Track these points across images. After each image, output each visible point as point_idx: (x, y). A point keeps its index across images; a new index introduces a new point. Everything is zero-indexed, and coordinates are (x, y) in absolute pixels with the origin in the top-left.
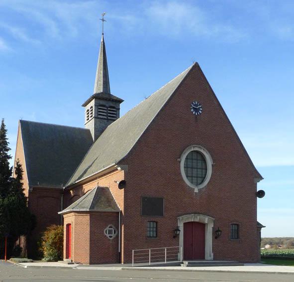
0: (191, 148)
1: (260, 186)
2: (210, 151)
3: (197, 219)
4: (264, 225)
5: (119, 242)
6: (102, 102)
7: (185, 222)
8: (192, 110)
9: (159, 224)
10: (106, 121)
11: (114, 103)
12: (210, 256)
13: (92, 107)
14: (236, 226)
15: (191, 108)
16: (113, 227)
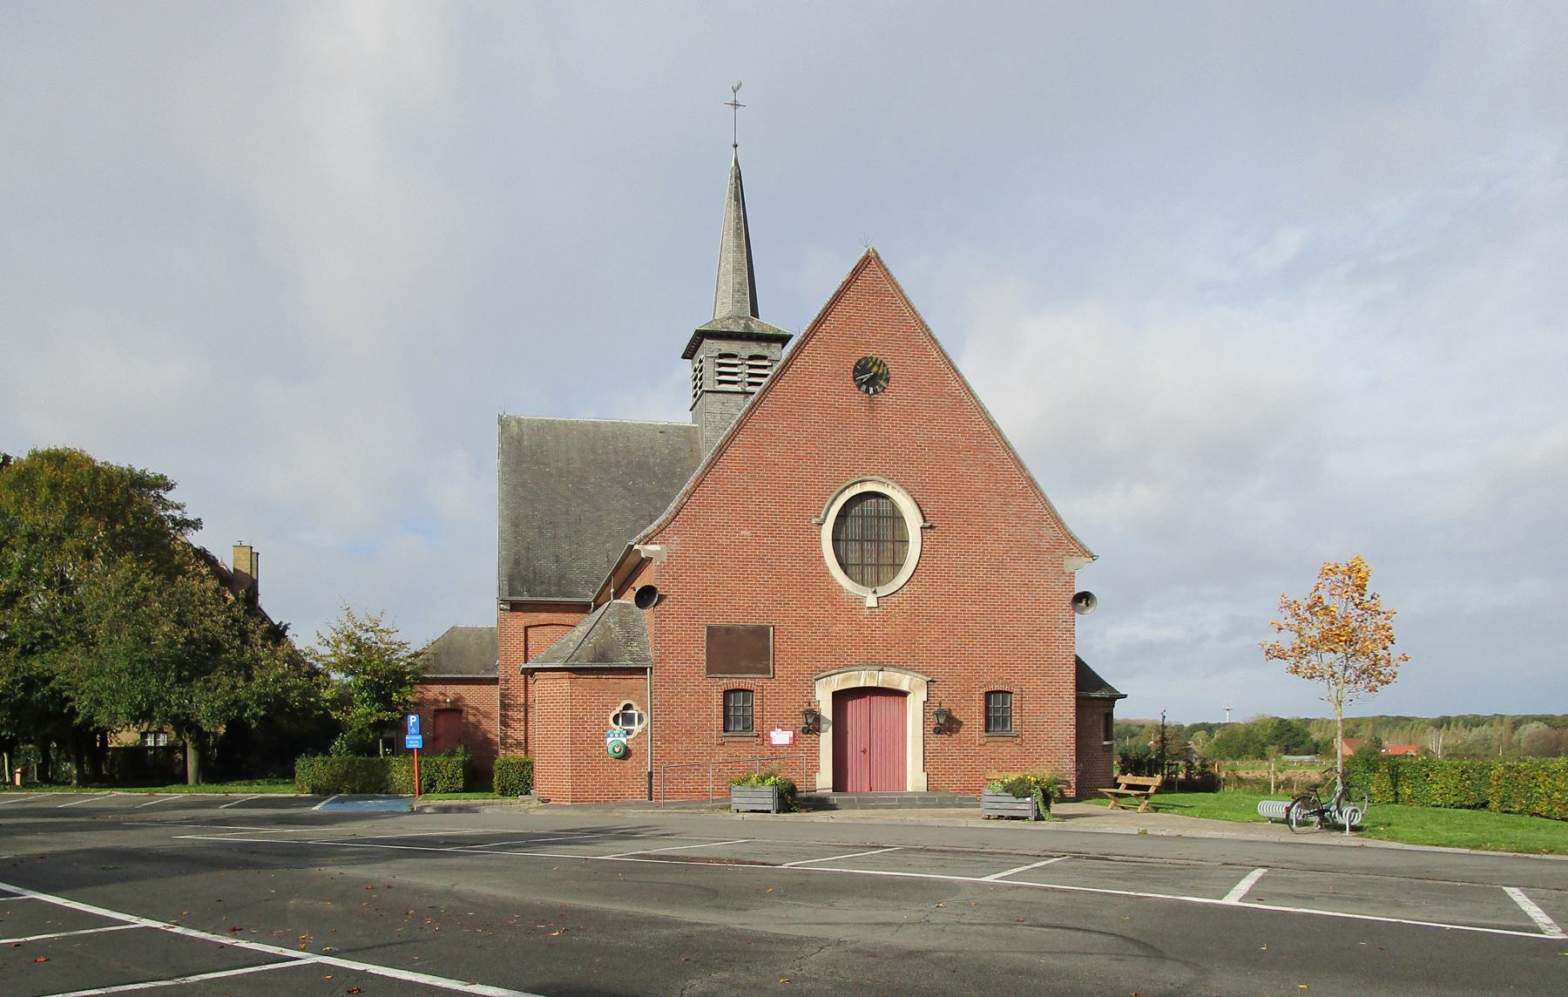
13: (701, 362)
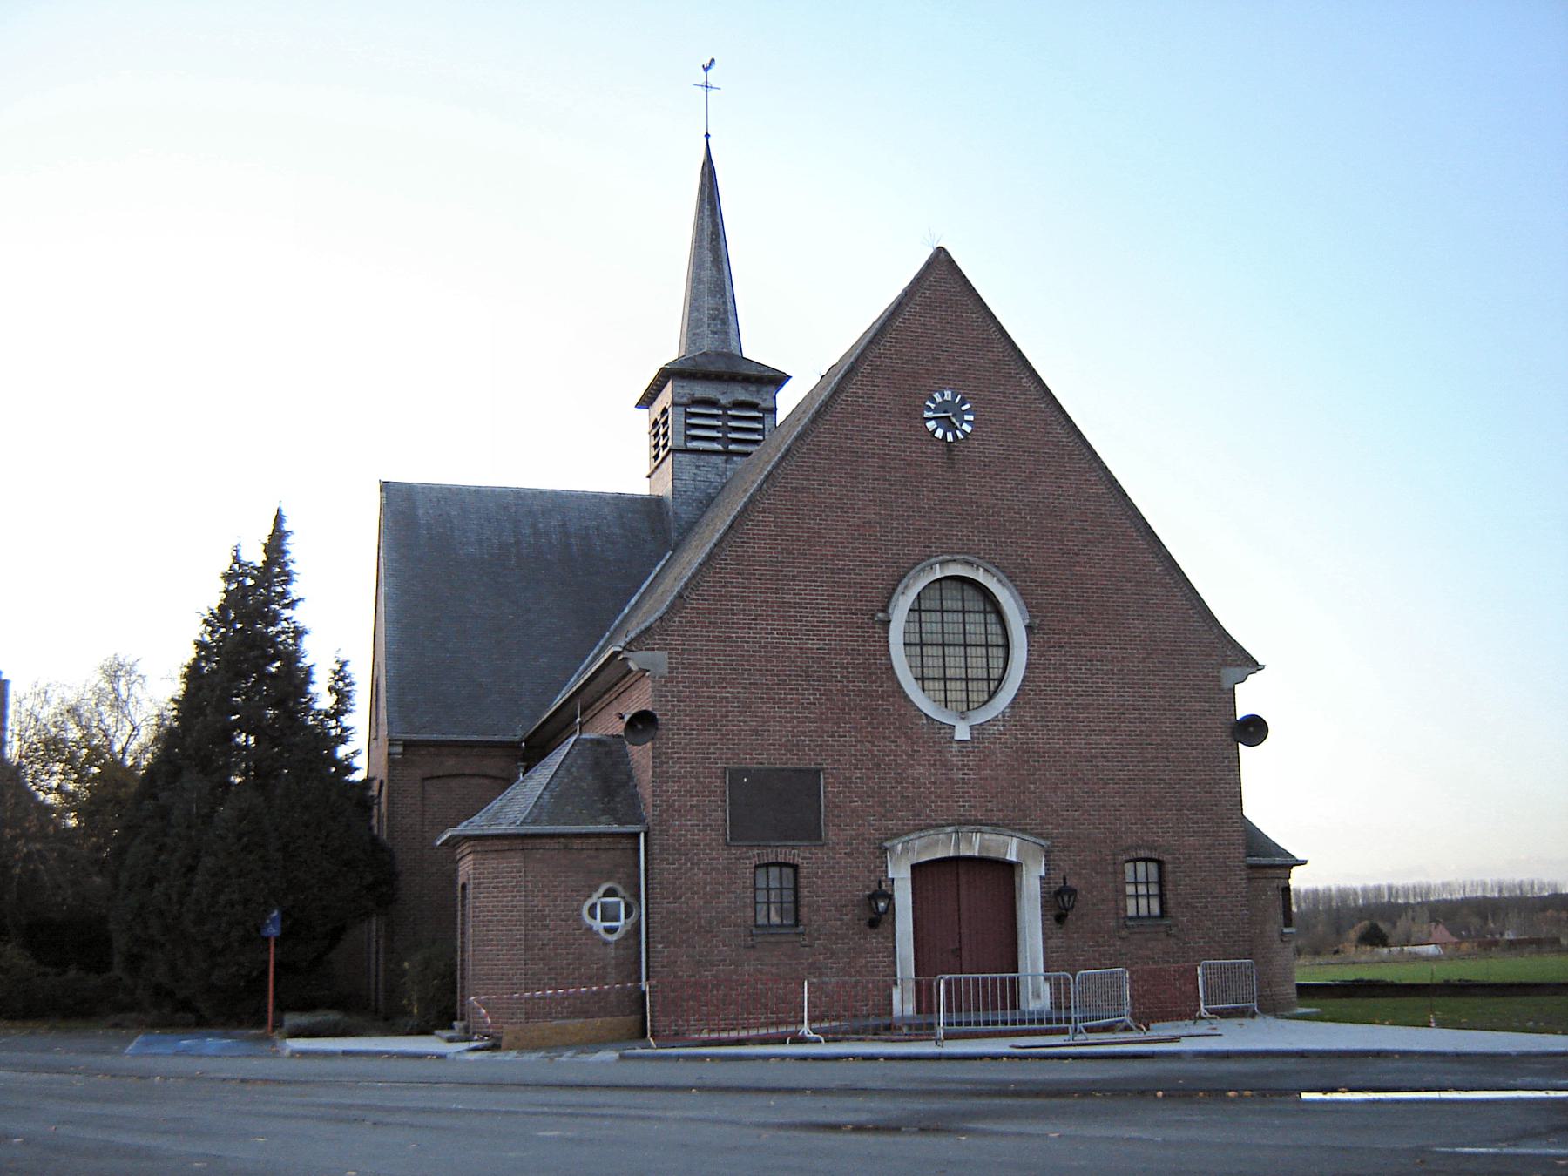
0: (931, 566)
1: (1249, 699)
2: (1010, 577)
3: (973, 846)
4: (1299, 857)
6: (701, 390)
7: (915, 861)
8: (931, 425)
9: (803, 873)
10: (719, 460)
11: (753, 388)
12: (1037, 995)
13: (665, 411)
14: (788, 872)
16: (620, 889)
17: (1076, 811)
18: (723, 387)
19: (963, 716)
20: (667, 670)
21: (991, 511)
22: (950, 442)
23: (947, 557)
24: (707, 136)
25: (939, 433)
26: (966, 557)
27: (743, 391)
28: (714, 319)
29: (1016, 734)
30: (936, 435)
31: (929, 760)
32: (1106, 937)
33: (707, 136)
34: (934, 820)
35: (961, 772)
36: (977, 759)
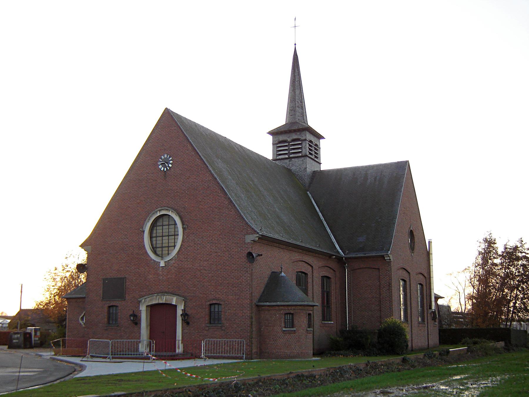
0: (157, 212)
3: (163, 300)
5: (152, 348)
8: (160, 167)
10: (287, 161)
15: (170, 165)
17: (195, 288)
18: (288, 135)
19: (162, 257)
20: (91, 251)
21: (176, 191)
22: (166, 171)
23: (160, 209)
24: (295, 44)
25: (163, 169)
26: (165, 208)
27: (295, 135)
28: (291, 111)
29: (178, 264)
30: (162, 170)
31: (153, 273)
32: (202, 330)
33: (295, 44)
34: (154, 292)
35: (162, 277)
36: (166, 272)
